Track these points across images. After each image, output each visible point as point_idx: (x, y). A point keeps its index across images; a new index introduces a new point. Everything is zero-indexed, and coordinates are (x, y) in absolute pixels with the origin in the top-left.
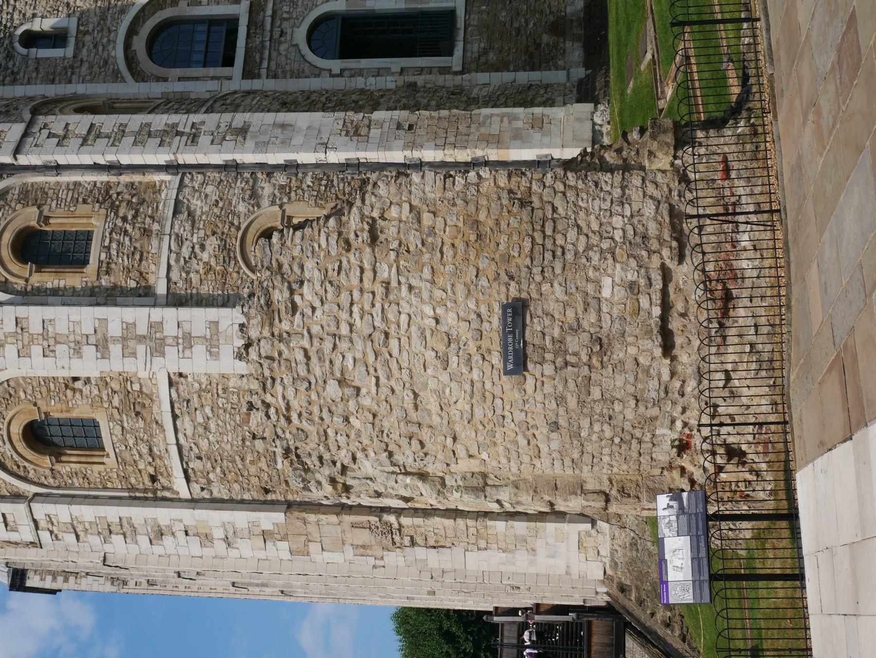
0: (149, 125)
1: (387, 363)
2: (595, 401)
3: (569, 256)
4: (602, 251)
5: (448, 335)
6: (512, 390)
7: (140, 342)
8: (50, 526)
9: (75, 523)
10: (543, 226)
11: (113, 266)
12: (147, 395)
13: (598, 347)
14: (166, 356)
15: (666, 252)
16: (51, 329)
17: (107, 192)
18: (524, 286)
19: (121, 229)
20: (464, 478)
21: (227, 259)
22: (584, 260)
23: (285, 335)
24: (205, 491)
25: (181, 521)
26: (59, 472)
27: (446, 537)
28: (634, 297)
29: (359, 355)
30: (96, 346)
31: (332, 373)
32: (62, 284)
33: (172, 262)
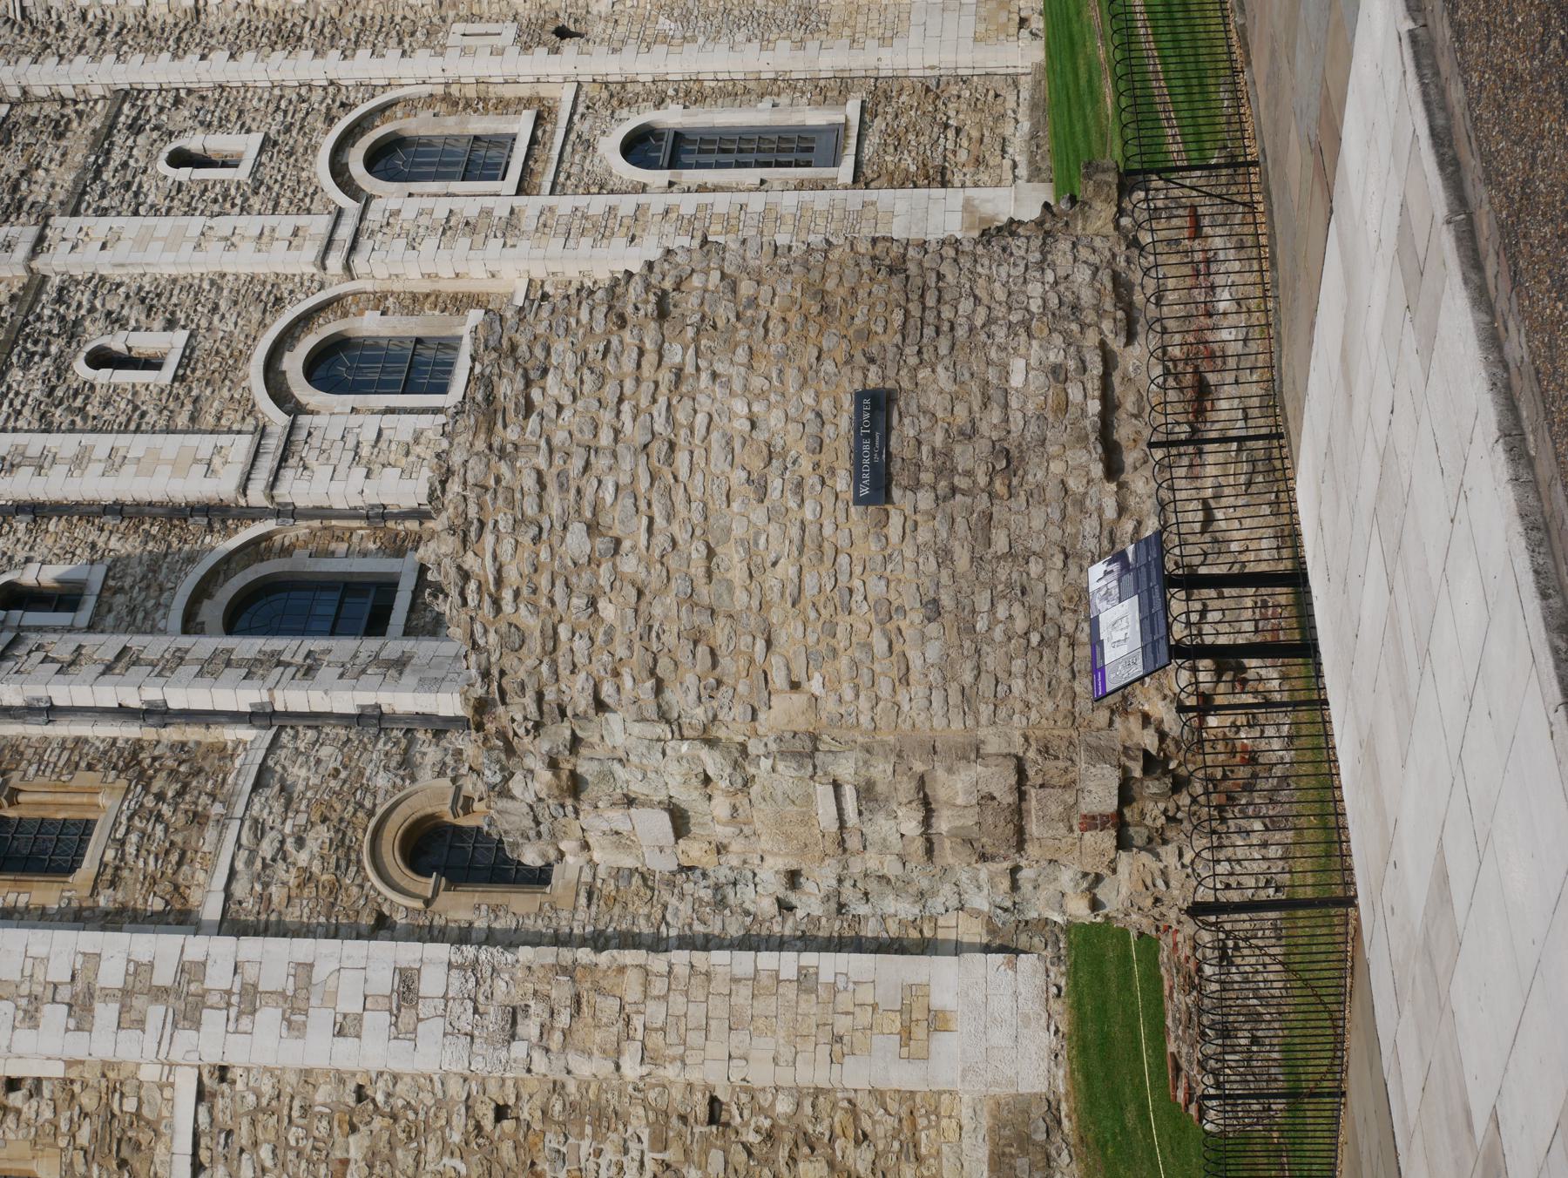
0: (230, 651)
2: (999, 558)
3: (961, 332)
4: (1010, 325)
5: (769, 445)
6: (866, 536)
7: (156, 999)
10: (922, 296)
11: (125, 873)
12: (148, 1123)
13: (1004, 463)
14: (203, 1029)
15: (1107, 325)
17: (134, 755)
18: (891, 372)
19: (151, 812)
20: (780, 739)
21: (343, 863)
22: (983, 337)
23: (509, 448)
29: (624, 479)
30: (70, 1006)
31: (578, 511)
32: (23, 900)
33: (240, 866)
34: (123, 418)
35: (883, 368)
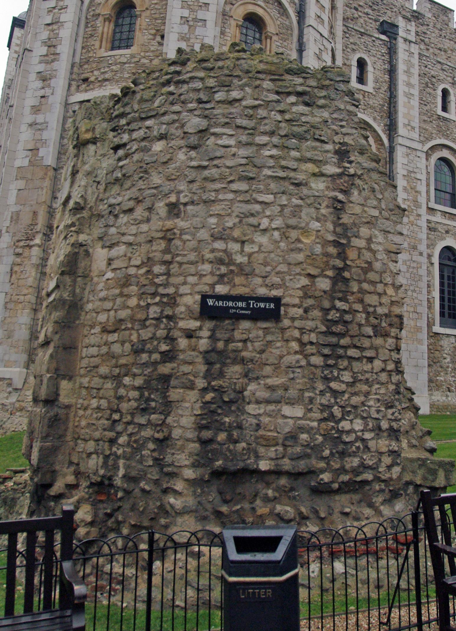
1: (222, 178)
4: (330, 407)
8: (59, 8)
9: (59, 24)
10: (355, 347)
16: (199, 24)
24: (72, 114)
25: (52, 94)
26: (97, 19)
27: (18, 279)
28: (280, 441)
34: (424, 99)
35: (301, 318)
